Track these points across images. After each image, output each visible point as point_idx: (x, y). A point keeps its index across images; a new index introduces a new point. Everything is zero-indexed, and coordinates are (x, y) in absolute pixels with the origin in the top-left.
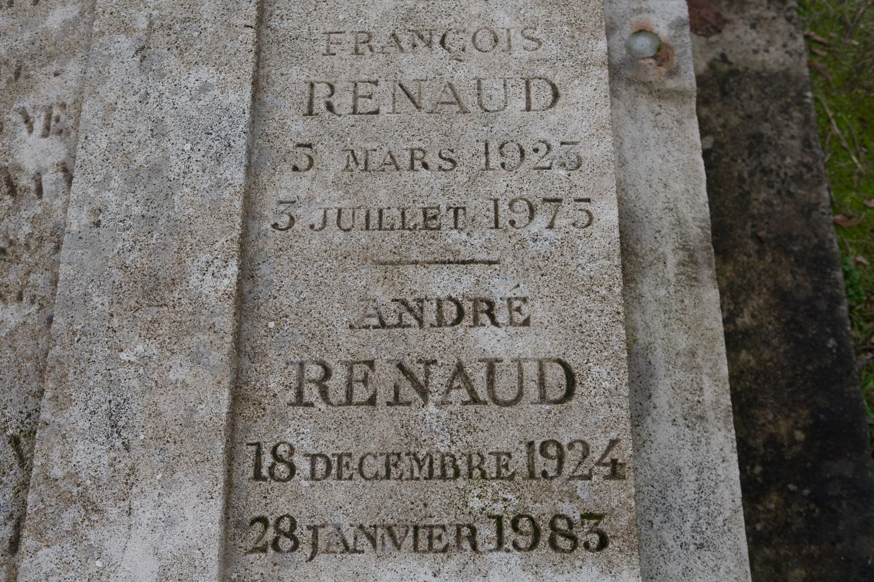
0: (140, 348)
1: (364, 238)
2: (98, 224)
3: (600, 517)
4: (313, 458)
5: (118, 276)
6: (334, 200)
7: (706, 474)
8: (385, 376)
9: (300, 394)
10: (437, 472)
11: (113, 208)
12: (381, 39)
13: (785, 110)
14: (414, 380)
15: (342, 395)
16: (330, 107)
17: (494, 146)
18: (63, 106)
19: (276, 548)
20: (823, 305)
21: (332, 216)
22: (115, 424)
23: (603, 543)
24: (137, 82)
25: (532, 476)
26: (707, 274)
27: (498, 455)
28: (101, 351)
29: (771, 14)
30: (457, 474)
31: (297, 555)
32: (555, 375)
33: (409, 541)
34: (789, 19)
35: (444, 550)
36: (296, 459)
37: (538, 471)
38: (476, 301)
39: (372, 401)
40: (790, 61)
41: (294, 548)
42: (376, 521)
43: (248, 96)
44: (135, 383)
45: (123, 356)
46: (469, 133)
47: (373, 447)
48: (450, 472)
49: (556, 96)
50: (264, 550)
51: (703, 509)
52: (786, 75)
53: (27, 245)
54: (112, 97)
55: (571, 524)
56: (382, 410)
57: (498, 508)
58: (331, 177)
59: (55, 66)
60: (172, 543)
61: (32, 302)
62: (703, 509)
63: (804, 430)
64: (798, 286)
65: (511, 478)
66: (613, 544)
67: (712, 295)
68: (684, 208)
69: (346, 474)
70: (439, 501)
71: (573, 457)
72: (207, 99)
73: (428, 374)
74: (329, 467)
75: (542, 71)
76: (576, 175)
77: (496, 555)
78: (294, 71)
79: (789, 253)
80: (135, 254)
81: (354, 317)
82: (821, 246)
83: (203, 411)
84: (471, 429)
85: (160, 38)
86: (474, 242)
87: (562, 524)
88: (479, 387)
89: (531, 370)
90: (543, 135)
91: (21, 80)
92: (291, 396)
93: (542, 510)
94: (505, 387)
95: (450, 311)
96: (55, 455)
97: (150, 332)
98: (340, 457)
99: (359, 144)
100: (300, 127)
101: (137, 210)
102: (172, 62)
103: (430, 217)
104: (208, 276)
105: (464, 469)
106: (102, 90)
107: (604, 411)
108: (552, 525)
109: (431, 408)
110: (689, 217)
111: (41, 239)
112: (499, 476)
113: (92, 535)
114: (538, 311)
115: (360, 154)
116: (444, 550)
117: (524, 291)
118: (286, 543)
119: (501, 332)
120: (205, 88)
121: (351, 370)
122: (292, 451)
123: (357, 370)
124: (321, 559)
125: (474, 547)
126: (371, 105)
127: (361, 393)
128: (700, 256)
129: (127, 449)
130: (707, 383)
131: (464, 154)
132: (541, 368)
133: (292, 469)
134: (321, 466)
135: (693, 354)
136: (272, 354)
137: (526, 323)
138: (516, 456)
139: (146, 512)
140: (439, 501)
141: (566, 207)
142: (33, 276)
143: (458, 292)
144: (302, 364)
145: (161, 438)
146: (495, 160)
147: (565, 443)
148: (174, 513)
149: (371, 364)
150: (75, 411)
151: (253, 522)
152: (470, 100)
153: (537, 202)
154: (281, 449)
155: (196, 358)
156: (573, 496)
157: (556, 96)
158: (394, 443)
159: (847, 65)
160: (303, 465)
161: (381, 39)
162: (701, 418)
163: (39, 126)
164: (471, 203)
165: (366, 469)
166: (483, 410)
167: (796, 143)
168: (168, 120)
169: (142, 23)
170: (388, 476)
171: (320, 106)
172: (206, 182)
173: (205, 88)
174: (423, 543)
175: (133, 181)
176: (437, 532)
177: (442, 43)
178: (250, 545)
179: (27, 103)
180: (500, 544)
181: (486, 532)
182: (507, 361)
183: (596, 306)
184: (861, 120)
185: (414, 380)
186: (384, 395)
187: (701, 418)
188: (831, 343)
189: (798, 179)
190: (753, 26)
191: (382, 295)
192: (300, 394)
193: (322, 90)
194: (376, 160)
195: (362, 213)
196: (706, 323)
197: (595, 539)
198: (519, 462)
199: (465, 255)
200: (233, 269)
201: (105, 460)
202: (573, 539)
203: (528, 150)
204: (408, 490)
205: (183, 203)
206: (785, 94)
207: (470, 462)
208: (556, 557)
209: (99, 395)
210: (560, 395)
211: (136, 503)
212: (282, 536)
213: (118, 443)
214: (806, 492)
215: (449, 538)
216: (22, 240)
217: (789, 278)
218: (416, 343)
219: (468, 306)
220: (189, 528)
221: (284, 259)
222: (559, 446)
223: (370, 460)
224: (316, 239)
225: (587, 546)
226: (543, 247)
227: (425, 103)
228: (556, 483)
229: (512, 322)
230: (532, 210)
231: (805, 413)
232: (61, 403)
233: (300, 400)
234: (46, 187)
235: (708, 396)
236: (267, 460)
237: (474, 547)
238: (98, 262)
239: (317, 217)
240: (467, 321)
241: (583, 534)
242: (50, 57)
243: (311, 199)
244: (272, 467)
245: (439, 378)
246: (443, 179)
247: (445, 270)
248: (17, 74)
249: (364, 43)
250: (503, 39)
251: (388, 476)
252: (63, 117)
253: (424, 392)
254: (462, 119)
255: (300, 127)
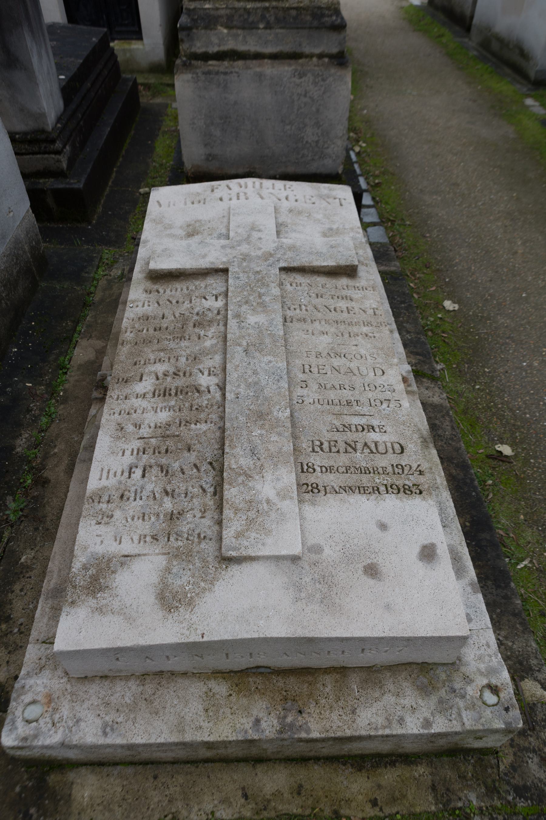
0: (259, 432)
1: (328, 407)
2: (238, 398)
3: (418, 486)
4: (321, 467)
5: (248, 412)
6: (317, 397)
7: (442, 505)
8: (342, 446)
9: (313, 449)
10: (363, 472)
11: (242, 393)
12: (324, 354)
13: (443, 416)
14: (351, 447)
15: (328, 450)
16: (310, 371)
17: (366, 385)
18: (215, 368)
19: (313, 492)
20: (468, 481)
21: (316, 401)
22: (253, 453)
23: (421, 493)
24: (246, 359)
25: (394, 474)
26: (431, 445)
27: (382, 468)
28: (245, 433)
29: (433, 386)
30: (370, 473)
31: (320, 494)
32: (397, 447)
33: (357, 490)
34: (439, 388)
35: (370, 493)
36: (315, 467)
37: (396, 472)
38: (368, 426)
39: (338, 452)
40: (442, 401)
41: (319, 491)
42: (345, 485)
43: (285, 364)
44: (259, 441)
45: (253, 434)
46: (358, 382)
47: (341, 464)
48: (368, 472)
49: (384, 373)
50: (308, 492)
51: (443, 515)
52: (441, 405)
53: (207, 407)
54: (237, 363)
55: (409, 487)
56: (342, 454)
57: (385, 482)
58: (314, 390)
59: (210, 356)
60: (280, 485)
61: (211, 423)
62: (443, 515)
63: (469, 522)
64: (458, 474)
65: (388, 474)
66: (424, 493)
67: (434, 452)
68: (420, 426)
69: (333, 472)
70: (365, 480)
71: (406, 469)
72: (271, 365)
73: (355, 445)
74: (327, 470)
75: (378, 366)
76: (394, 394)
77: (387, 495)
78: (297, 361)
79: (453, 463)
80: (253, 406)
81: (329, 428)
82: (464, 461)
83: (285, 449)
84: (372, 460)
85: (251, 348)
86: (365, 410)
87: (406, 487)
88: (373, 449)
89: (389, 445)
90: (381, 382)
91: (197, 360)
92: (311, 449)
93: (400, 483)
94: (381, 449)
95: (360, 428)
96: (233, 462)
97: (262, 427)
98: (330, 467)
99: (322, 382)
100: (301, 376)
101: (252, 394)
102: (257, 354)
103: (349, 403)
104: (280, 412)
105: (372, 471)
106: (233, 361)
107: (414, 457)
108: (403, 487)
109: (358, 454)
110: (422, 428)
111: (212, 405)
112: (384, 473)
113: (250, 484)
114: (388, 429)
115: (323, 385)
116: (370, 493)
117: (382, 423)
118: (316, 491)
119: (377, 434)
120: (270, 362)
121: (330, 443)
122: (313, 465)
123: (332, 443)
124: (328, 495)
125: (379, 493)
126: (324, 372)
127: (334, 449)
128: (428, 440)
129: (259, 459)
130: (437, 478)
131: (357, 386)
132: (392, 444)
133: (314, 470)
134: (324, 469)
135: (431, 469)
136: (302, 438)
137: (385, 432)
138: (388, 468)
139: (269, 476)
140: (365, 480)
141: (392, 402)
142: (210, 416)
143: (362, 423)
144: (312, 441)
145: (271, 457)
146: (367, 388)
147: (404, 465)
148: (279, 477)
149: (336, 441)
150: (238, 449)
151: (303, 484)
152: (356, 372)
153: (383, 400)
154: (310, 464)
155: (279, 434)
156: (409, 480)
157: (384, 373)
158: (347, 463)
159: (462, 407)
160: (318, 469)
161: (324, 354)
162: (437, 488)
163: (206, 373)
164: (361, 399)
165: (339, 470)
166: (376, 455)
167: (449, 428)
168: (258, 370)
169: (245, 343)
170: (347, 473)
171: (307, 370)
172: (275, 387)
173: (270, 362)
174: (362, 491)
175: (249, 386)
176: (366, 488)
177: (344, 356)
178: (304, 491)
179: (201, 367)
180: (387, 493)
181: (382, 489)
182: (381, 442)
183: (407, 428)
184: (471, 425)
185: (351, 447)
186: (342, 450)
187: (437, 488)
188: (474, 494)
189: (452, 439)
190: (427, 389)
191: (337, 423)
192: (313, 449)
193: (307, 367)
194: (328, 386)
195: (326, 400)
196: (434, 460)
197: (418, 491)
198: (390, 469)
199: (362, 413)
200: (288, 410)
201: (252, 463)
202: (412, 492)
203: (377, 386)
204: (354, 476)
205: (267, 392)
206: (442, 411)
207: (373, 469)
208: (407, 496)
209: (246, 445)
210: (400, 452)
211: (265, 474)
212: (314, 489)
213: (255, 458)
214: (474, 543)
215: (370, 490)
216: (204, 405)
217: (454, 471)
218: (350, 436)
219: (365, 427)
220: (285, 481)
221: (302, 411)
222: (402, 466)
223: (340, 468)
224: (312, 407)
225: (416, 493)
226: (387, 412)
227: (342, 371)
228: (403, 476)
229: (380, 432)
230: (382, 403)
231: (468, 516)
232: (232, 447)
233: (313, 451)
234: (211, 390)
235: (439, 481)
236: (305, 467)
237: (379, 493)
238: (240, 408)
239: (311, 401)
240: (366, 431)
241: (414, 489)
242: (207, 354)
243: (308, 396)
244: (307, 470)
245: (359, 446)
246: (351, 393)
247: (356, 417)
248: (195, 359)
249: (319, 355)
250: (364, 356)
251: (347, 473)
252: (215, 371)
253: (355, 450)
254: (354, 377)
255: (301, 376)
